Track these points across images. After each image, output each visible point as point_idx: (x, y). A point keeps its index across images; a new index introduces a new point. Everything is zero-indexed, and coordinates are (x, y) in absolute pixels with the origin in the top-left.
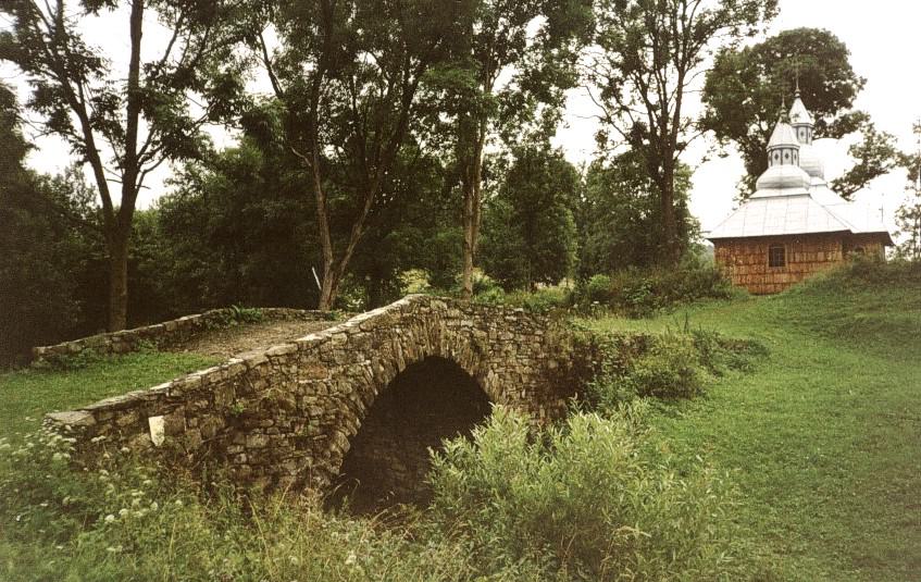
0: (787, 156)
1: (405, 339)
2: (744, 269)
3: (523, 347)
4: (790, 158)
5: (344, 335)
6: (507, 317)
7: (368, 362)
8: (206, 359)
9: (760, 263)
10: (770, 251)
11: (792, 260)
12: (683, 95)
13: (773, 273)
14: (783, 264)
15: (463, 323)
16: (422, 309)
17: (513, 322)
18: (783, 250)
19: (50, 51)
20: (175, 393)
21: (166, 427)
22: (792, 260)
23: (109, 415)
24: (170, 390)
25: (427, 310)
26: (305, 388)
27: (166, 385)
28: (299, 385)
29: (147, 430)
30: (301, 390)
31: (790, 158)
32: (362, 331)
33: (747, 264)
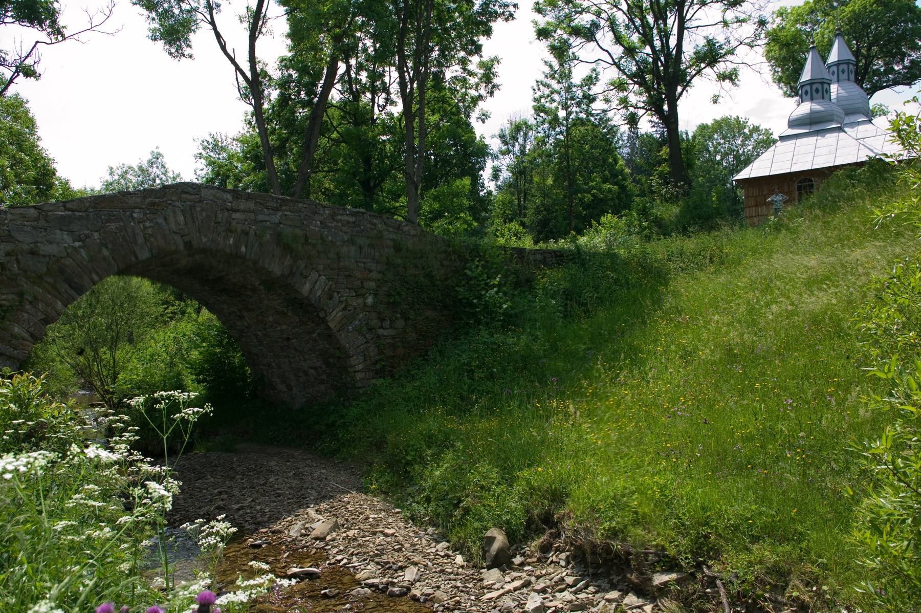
4: (820, 92)
6: (340, 217)
15: (260, 217)
17: (348, 223)
31: (820, 92)
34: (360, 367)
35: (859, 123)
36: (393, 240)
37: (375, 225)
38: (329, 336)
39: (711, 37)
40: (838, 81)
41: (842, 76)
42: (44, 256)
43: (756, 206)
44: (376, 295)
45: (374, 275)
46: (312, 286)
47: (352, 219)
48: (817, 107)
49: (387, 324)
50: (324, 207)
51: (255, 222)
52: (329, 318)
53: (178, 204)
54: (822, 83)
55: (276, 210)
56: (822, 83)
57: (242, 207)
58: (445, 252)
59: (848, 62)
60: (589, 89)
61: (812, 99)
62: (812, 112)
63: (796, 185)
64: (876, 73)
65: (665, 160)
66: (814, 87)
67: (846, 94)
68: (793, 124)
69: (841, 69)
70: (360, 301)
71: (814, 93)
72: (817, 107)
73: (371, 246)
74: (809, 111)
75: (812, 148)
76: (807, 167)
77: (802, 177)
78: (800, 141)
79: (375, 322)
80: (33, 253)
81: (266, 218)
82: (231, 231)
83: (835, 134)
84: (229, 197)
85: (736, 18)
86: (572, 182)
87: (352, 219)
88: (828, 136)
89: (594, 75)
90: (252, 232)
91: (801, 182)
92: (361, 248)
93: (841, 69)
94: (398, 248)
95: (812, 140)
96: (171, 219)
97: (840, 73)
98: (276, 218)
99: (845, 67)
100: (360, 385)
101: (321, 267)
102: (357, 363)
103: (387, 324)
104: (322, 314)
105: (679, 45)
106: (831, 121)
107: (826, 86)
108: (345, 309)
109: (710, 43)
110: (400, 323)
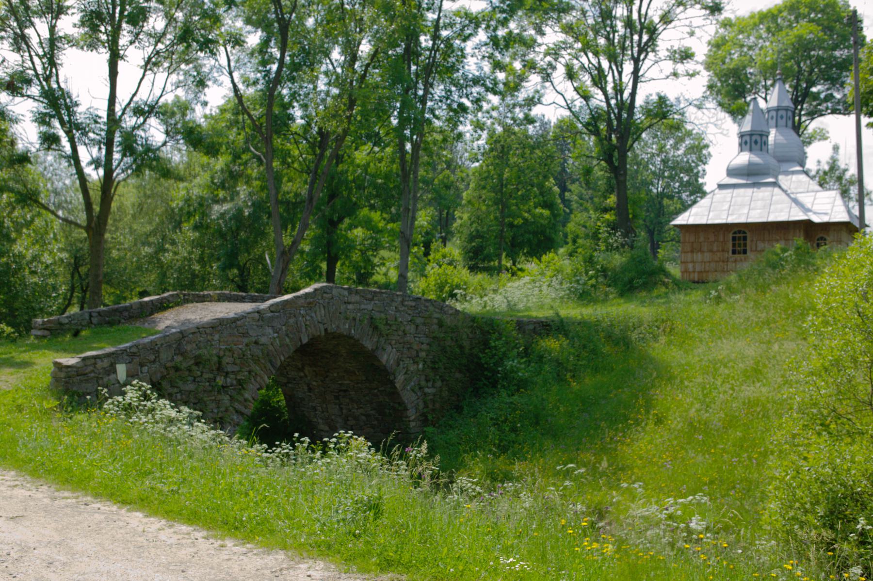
0: (756, 142)
1: (308, 318)
2: (707, 256)
3: (421, 327)
4: (759, 144)
5: (256, 315)
6: (406, 303)
7: (276, 335)
8: (316, 185)
9: (723, 251)
10: (734, 239)
11: (754, 248)
12: (639, 85)
13: (735, 261)
14: (745, 252)
15: (363, 307)
16: (325, 295)
18: (745, 238)
19: (44, 83)
20: (134, 350)
21: (127, 371)
22: (754, 248)
23: (93, 361)
24: (130, 347)
25: (329, 296)
26: (224, 351)
27: (127, 345)
28: (220, 349)
29: (115, 372)
30: (222, 353)
31: (759, 144)
32: (272, 312)
33: (711, 251)
34: (412, 418)
35: (793, 173)
36: (437, 318)
37: (427, 307)
38: (394, 394)
39: (662, 94)
40: (776, 126)
41: (782, 122)
42: (263, 345)
43: (692, 252)
44: (425, 362)
45: (425, 347)
46: (388, 357)
47: (413, 304)
48: (756, 159)
49: (430, 384)
50: (397, 295)
51: (360, 310)
52: (396, 381)
53: (321, 301)
54: (761, 135)
55: (372, 299)
56: (761, 135)
57: (353, 300)
58: (472, 326)
59: (786, 109)
60: (530, 110)
61: (751, 150)
62: (750, 164)
63: (731, 235)
64: (816, 96)
65: (611, 209)
66: (754, 138)
67: (785, 142)
68: (732, 172)
69: (779, 115)
70: (415, 367)
71: (753, 144)
72: (756, 159)
73: (424, 324)
74: (747, 163)
75: (748, 199)
76: (742, 220)
77: (736, 229)
78: (737, 191)
79: (423, 383)
80: (256, 343)
81: (365, 307)
82: (347, 319)
83: (770, 189)
84: (346, 293)
85: (687, 71)
86: (505, 206)
87: (413, 304)
88: (763, 189)
89: (537, 96)
90: (358, 318)
91: (735, 233)
92: (417, 326)
93: (779, 115)
94: (441, 324)
95: (749, 191)
96: (318, 313)
97: (779, 119)
98: (370, 307)
99: (783, 113)
100: (413, 431)
101: (394, 342)
102: (412, 414)
103: (430, 384)
104: (392, 378)
105: (633, 94)
106: (766, 174)
107: (764, 138)
108: (406, 373)
109: (662, 100)
110: (439, 384)
